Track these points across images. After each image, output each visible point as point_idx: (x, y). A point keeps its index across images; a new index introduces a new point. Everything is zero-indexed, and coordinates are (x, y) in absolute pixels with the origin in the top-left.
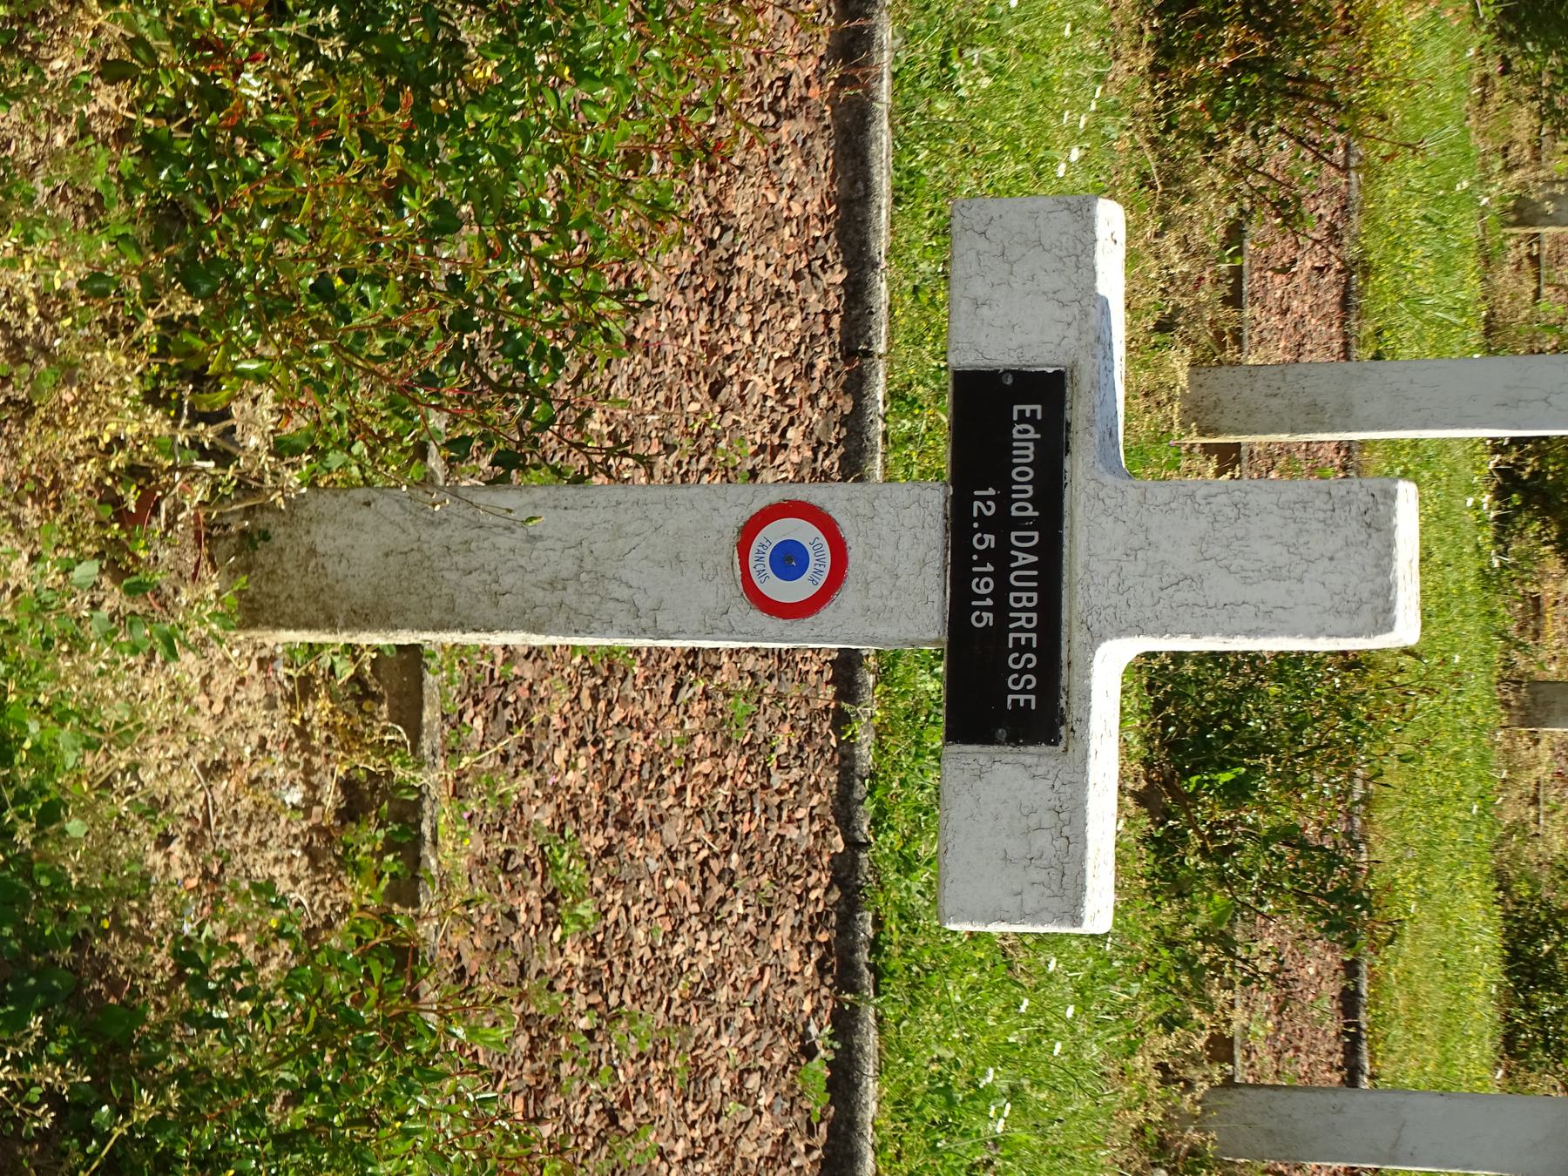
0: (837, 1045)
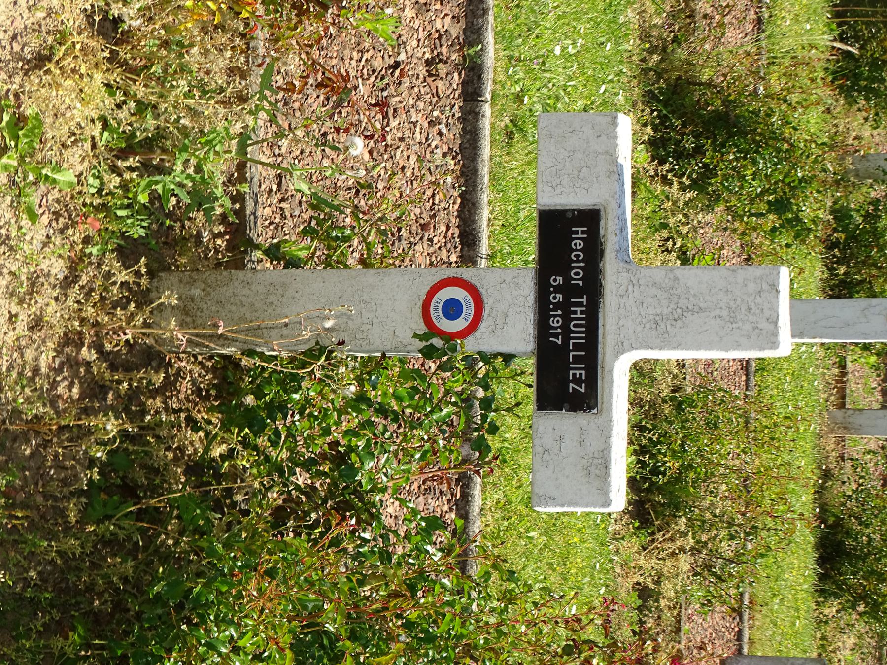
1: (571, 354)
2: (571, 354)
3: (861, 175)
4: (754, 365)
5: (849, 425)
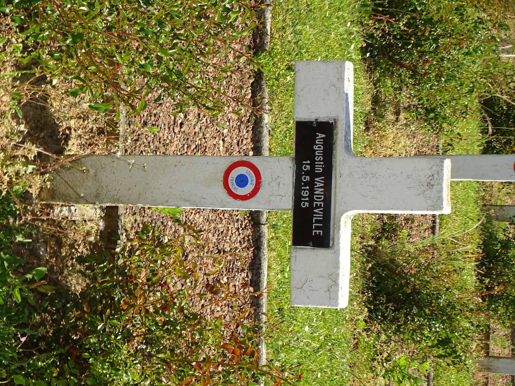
0: (76, 34)
1: (314, 225)
2: (314, 225)
3: (500, 219)
4: (432, 374)
5: (491, 367)
